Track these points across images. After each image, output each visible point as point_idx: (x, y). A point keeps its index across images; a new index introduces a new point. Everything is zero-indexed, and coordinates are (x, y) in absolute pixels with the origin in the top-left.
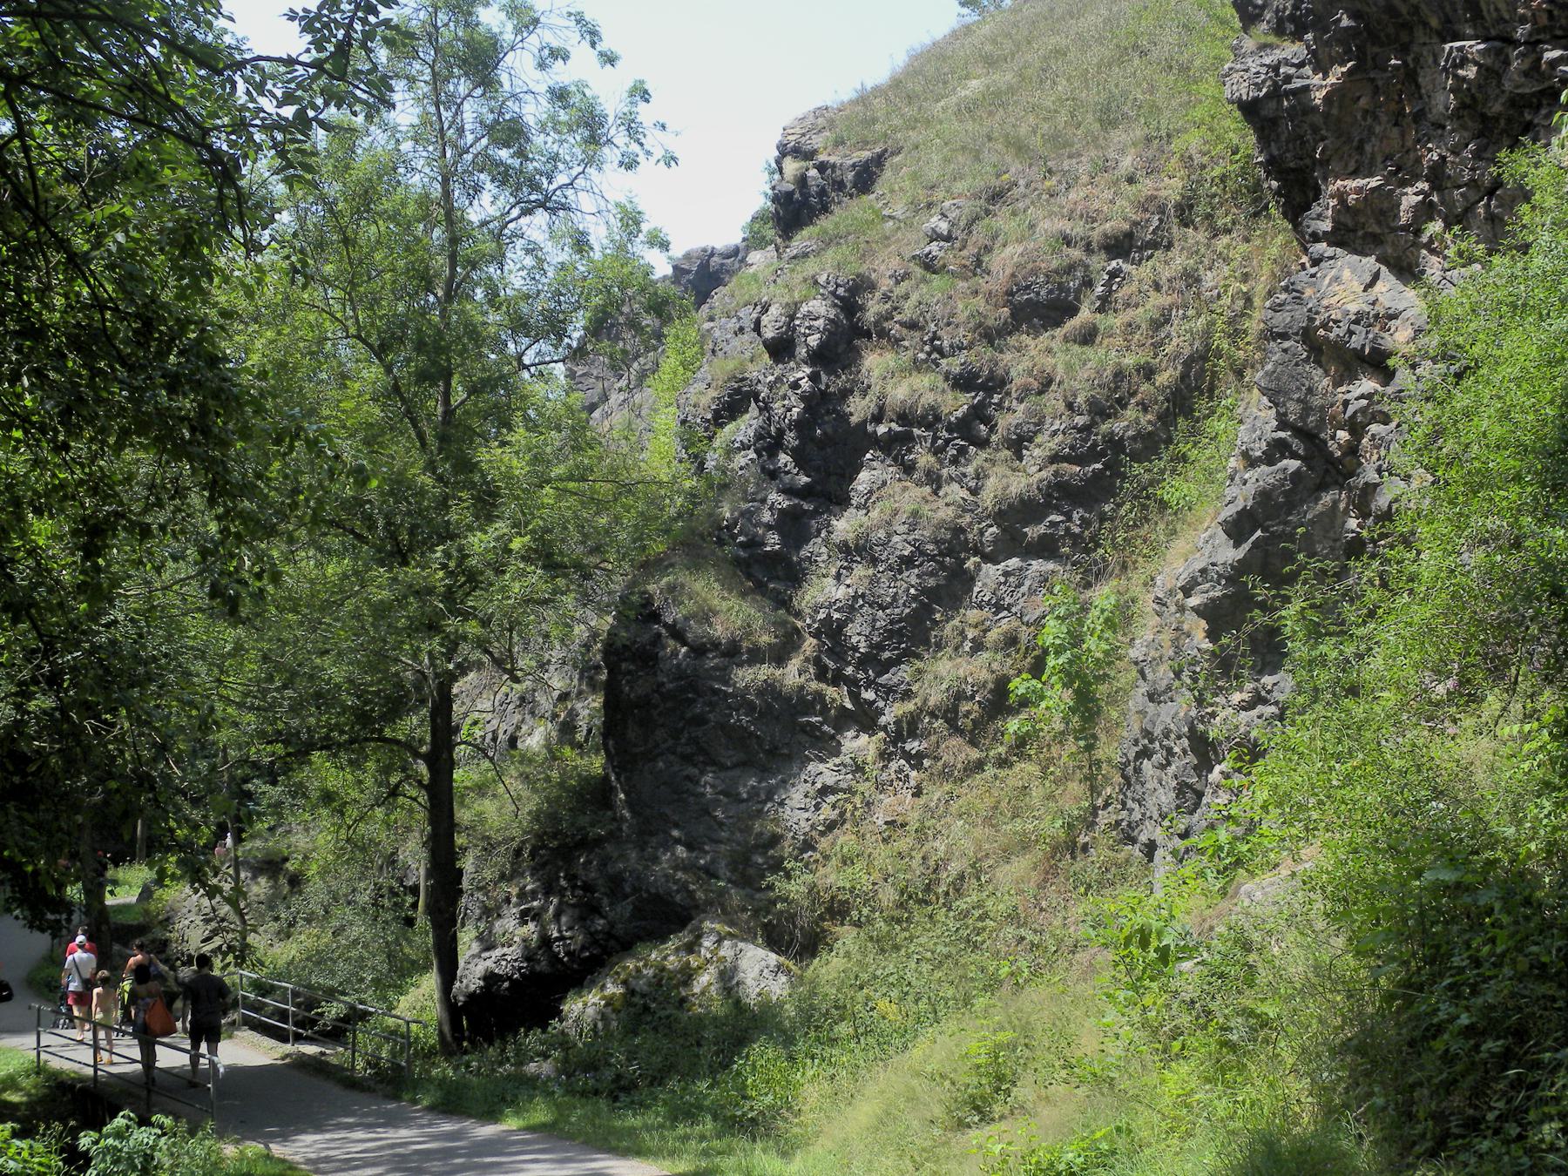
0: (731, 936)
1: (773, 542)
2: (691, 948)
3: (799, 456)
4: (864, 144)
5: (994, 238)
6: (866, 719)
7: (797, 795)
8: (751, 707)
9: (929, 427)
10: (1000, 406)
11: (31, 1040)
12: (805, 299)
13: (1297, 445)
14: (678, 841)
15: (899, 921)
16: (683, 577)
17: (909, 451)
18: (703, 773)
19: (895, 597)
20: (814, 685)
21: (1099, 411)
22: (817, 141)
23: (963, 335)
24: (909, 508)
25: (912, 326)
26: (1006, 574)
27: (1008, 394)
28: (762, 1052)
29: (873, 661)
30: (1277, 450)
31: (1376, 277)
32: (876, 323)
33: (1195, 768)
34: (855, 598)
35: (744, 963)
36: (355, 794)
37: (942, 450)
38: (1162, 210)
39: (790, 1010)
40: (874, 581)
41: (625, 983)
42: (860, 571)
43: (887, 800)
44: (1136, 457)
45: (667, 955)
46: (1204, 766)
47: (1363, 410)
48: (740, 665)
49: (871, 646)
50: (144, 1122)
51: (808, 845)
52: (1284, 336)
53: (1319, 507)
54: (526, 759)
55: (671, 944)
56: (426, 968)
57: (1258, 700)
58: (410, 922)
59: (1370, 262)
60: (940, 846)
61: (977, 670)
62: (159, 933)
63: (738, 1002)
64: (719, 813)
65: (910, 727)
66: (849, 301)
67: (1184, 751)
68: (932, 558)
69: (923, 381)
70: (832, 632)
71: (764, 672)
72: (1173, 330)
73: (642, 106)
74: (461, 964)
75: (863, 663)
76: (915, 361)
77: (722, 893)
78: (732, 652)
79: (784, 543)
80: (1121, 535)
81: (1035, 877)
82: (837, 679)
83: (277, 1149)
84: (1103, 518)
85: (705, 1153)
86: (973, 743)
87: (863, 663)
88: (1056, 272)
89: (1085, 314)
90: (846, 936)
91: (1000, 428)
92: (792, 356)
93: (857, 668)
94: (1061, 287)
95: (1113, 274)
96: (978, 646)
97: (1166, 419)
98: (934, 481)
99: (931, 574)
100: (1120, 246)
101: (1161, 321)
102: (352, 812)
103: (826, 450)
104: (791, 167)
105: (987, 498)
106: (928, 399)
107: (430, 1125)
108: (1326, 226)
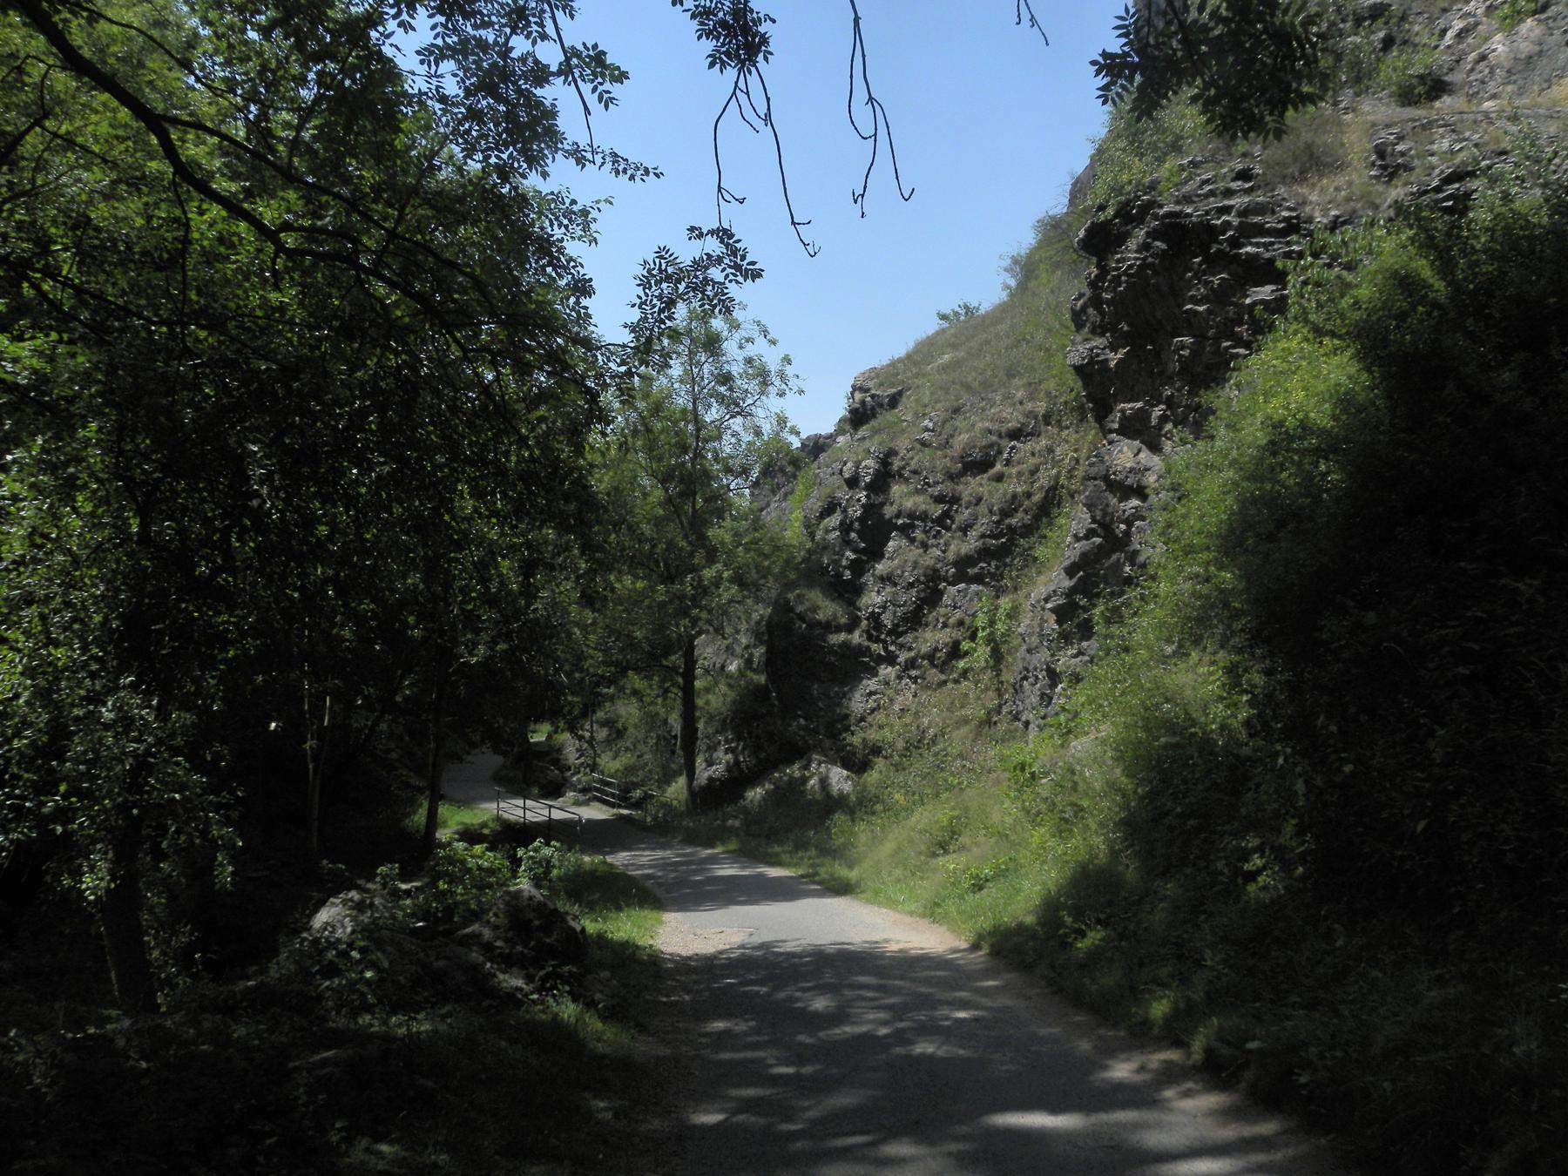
1: (847, 575)
2: (806, 767)
6: (891, 659)
7: (857, 696)
11: (494, 805)
16: (805, 591)
21: (1005, 513)
22: (871, 384)
23: (940, 477)
25: (915, 472)
28: (840, 818)
29: (895, 632)
30: (1090, 533)
31: (1140, 450)
38: (1036, 418)
44: (1022, 536)
45: (795, 770)
46: (1053, 685)
50: (548, 844)
51: (863, 719)
54: (729, 676)
55: (797, 766)
57: (1080, 653)
58: (673, 752)
62: (555, 755)
65: (911, 664)
66: (885, 460)
69: (920, 499)
70: (875, 618)
71: (842, 636)
75: (890, 633)
78: (829, 627)
80: (1014, 573)
83: (609, 859)
84: (1006, 565)
86: (942, 672)
87: (890, 633)
89: (998, 467)
90: (880, 763)
94: (987, 454)
95: (1013, 448)
96: (945, 625)
97: (1037, 518)
98: (925, 546)
100: (1015, 434)
103: (873, 532)
104: (858, 396)
105: (951, 556)
106: (923, 507)
108: (1116, 426)
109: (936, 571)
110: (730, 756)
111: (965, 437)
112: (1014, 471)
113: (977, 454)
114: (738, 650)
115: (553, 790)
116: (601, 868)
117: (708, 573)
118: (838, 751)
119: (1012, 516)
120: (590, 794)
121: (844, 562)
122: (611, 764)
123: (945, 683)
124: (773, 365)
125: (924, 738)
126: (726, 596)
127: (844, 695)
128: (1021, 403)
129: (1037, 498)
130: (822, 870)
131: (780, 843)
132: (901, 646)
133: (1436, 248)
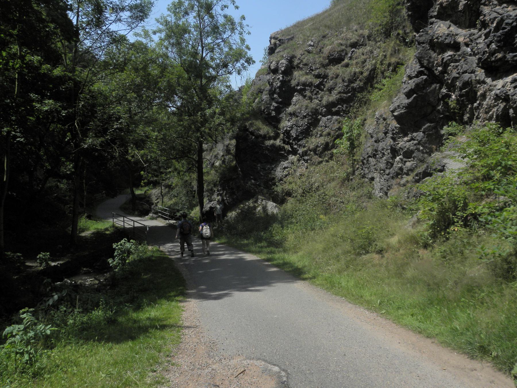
0: (265, 199)
1: (273, 114)
2: (256, 202)
3: (279, 94)
4: (289, 35)
5: (324, 45)
6: (294, 152)
7: (279, 169)
8: (268, 150)
9: (310, 87)
10: (326, 82)
11: (112, 220)
12: (281, 60)
13: (426, 72)
14: (252, 179)
15: (303, 196)
16: (254, 121)
17: (305, 92)
18: (258, 164)
19: (302, 125)
20: (283, 145)
21: (351, 81)
22: (278, 36)
23: (318, 66)
24: (305, 104)
25: (306, 65)
26: (328, 119)
27: (328, 79)
28: (276, 226)
29: (297, 139)
30: (420, 73)
31: (450, 26)
32: (297, 65)
33: (391, 158)
34: (293, 125)
35: (268, 205)
36: (182, 169)
37: (313, 92)
38: (364, 37)
39: (279, 216)
40: (297, 121)
41: (241, 209)
42: (294, 119)
43: (299, 170)
44: (358, 92)
45: (250, 203)
46: (394, 157)
47: (449, 60)
48: (266, 140)
49: (296, 136)
50: (129, 241)
51: (281, 180)
52: (423, 43)
53: (431, 88)
54: (216, 167)
55: (251, 201)
56: (198, 206)
57: (412, 139)
58: (194, 197)
59: (448, 22)
60: (313, 180)
61: (321, 141)
62: (147, 199)
63: (267, 214)
64: (262, 173)
65: (305, 153)
66: (290, 61)
67: (389, 154)
68: (310, 116)
69: (309, 77)
70: (287, 133)
71: (272, 142)
72: (367, 63)
73: (244, 21)
74: (205, 205)
75: (294, 139)
76: (306, 72)
77: (262, 190)
78: (265, 137)
79: (276, 113)
80: (355, 110)
81: (338, 186)
82: (288, 143)
83: (162, 248)
84: (351, 106)
85: (268, 253)
86: (320, 157)
87: (294, 139)
88: (340, 51)
89: (346, 61)
90: (291, 200)
91: (326, 87)
92: (278, 73)
93: (293, 141)
94: (341, 55)
95: (353, 52)
96: (321, 135)
97: (365, 84)
98: (311, 99)
99: (310, 119)
100: (354, 45)
101: (364, 62)
102: (182, 173)
103: (285, 93)
104: (273, 41)
105: (324, 102)
106: (310, 80)
107: (198, 242)
108: (436, 13)
109: (317, 110)
110: (219, 197)
111: (329, 47)
112: (354, 62)
113: (336, 55)
114: (219, 157)
115: (143, 213)
116: (155, 255)
117: (208, 112)
118: (270, 194)
119: (354, 83)
120: (160, 215)
121: (272, 108)
122: (169, 202)
123: (321, 162)
124: (237, 20)
125: (312, 188)
126: (217, 121)
127: (272, 169)
128: (356, 31)
129: (366, 74)
130: (277, 256)
131: (247, 238)
132: (300, 146)
133: (395, 68)
